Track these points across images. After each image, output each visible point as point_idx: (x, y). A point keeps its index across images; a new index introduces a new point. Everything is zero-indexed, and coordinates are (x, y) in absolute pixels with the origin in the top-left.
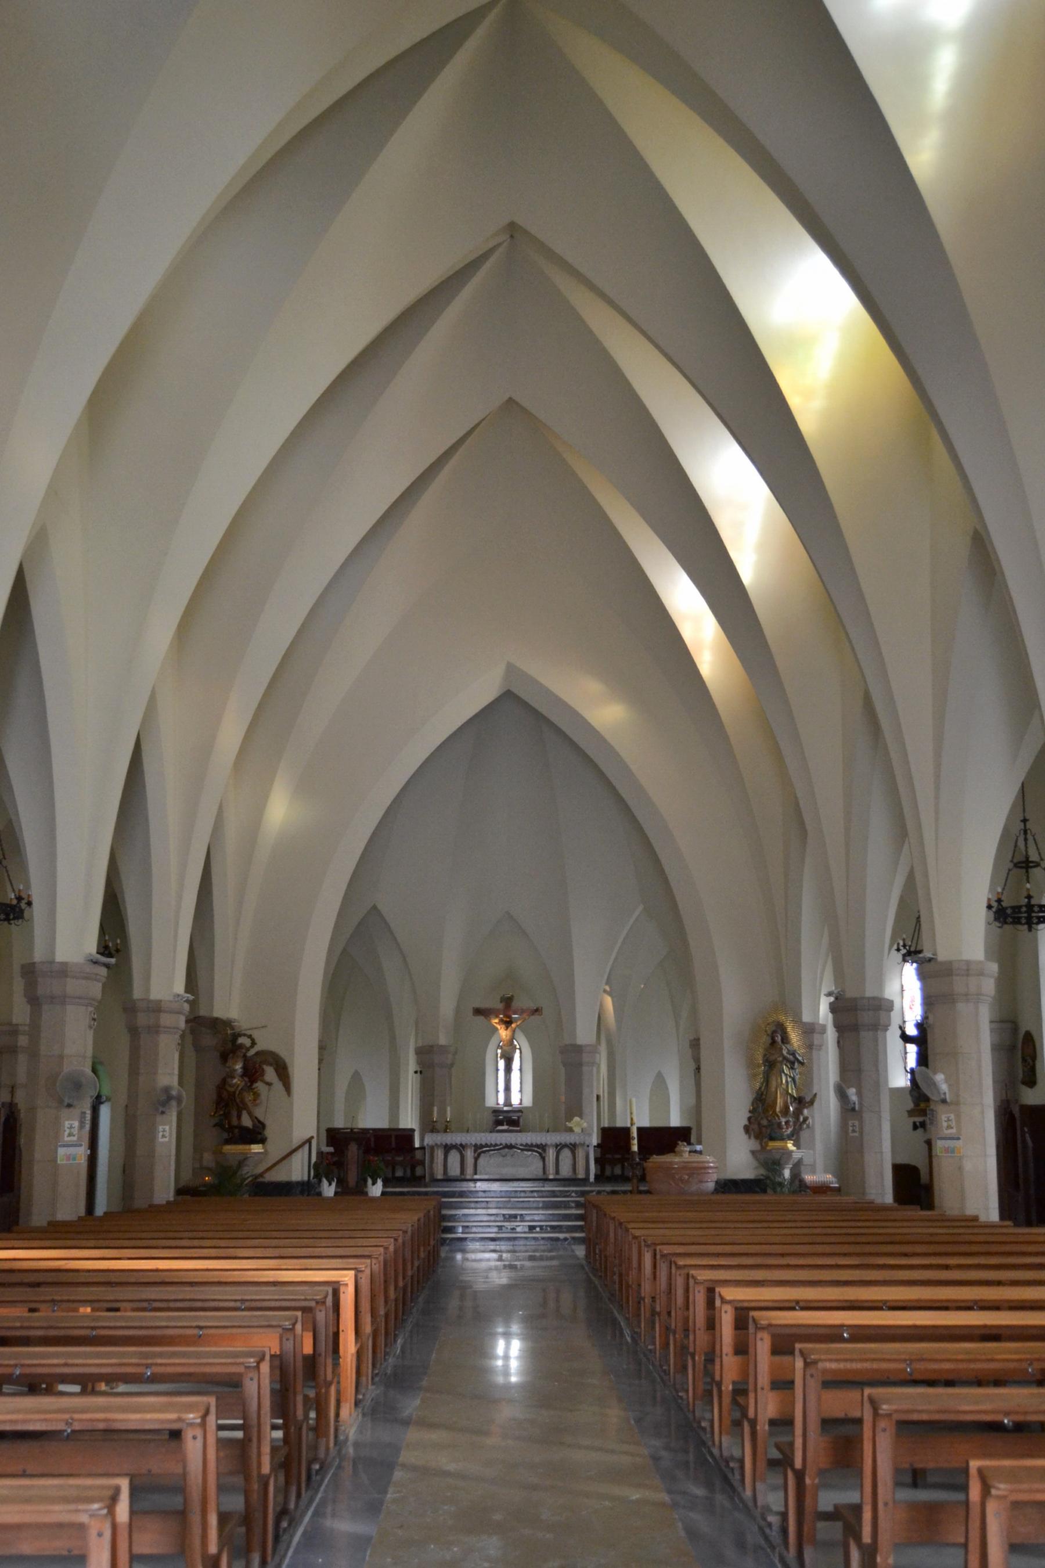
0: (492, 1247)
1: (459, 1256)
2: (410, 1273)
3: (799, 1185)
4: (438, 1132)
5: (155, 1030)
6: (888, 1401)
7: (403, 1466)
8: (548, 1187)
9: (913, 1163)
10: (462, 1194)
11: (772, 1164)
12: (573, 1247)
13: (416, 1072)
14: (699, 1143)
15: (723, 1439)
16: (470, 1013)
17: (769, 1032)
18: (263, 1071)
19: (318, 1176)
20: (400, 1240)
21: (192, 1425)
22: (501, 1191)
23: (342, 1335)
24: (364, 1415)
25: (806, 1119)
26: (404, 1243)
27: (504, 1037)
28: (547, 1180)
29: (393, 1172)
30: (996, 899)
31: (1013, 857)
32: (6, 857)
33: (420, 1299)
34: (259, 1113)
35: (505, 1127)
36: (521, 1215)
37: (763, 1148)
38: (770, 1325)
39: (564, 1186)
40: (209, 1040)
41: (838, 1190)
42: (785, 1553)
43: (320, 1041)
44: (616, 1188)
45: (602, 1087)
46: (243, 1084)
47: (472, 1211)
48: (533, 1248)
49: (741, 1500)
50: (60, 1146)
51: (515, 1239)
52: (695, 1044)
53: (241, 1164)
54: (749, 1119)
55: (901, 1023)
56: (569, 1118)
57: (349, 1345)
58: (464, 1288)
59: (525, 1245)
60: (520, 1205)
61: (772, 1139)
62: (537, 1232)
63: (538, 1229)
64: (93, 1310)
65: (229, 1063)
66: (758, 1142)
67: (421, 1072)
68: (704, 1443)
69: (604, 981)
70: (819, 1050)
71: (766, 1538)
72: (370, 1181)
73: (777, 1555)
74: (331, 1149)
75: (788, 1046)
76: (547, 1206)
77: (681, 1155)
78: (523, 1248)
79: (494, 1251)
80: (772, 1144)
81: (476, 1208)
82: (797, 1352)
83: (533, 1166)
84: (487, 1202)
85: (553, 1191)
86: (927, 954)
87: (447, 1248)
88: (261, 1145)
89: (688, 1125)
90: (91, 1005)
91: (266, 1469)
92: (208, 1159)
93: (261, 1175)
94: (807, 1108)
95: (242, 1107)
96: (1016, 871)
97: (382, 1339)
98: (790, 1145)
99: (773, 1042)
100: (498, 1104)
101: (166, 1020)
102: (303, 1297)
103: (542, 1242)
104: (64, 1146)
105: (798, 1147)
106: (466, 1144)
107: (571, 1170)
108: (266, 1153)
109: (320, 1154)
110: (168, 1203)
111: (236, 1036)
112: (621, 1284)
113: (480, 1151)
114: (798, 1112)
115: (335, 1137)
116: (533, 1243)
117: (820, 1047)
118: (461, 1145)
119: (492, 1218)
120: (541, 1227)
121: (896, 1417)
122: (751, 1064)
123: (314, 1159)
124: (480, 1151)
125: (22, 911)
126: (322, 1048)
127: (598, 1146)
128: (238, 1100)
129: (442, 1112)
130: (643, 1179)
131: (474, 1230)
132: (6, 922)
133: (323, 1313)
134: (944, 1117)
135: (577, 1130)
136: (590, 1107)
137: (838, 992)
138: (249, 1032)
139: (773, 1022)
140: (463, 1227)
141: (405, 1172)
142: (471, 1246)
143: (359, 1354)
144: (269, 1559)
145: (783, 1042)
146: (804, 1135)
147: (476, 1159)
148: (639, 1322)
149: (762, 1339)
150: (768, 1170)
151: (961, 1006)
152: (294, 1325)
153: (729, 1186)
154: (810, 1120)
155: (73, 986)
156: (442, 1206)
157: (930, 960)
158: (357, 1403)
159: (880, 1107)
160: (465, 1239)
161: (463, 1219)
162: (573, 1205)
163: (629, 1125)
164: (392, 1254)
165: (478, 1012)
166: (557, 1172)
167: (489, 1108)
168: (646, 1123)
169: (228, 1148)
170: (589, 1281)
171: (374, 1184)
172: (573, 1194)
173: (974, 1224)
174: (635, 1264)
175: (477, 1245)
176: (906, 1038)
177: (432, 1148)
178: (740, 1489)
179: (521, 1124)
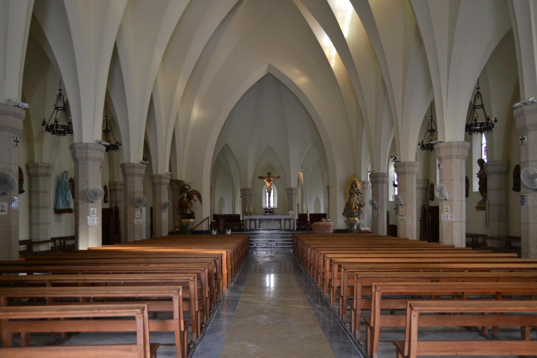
0: (265, 250)
1: (255, 253)
2: (240, 255)
3: (360, 231)
4: (248, 215)
5: (160, 184)
6: (360, 275)
7: (241, 301)
8: (282, 232)
9: (395, 224)
10: (255, 234)
11: (351, 225)
12: (290, 250)
13: (240, 197)
14: (329, 218)
15: (327, 294)
16: (257, 178)
17: (351, 184)
18: (193, 197)
19: (211, 229)
20: (238, 245)
21: (191, 280)
22: (267, 233)
23: (223, 268)
24: (229, 291)
25: (362, 211)
26: (239, 246)
27: (268, 185)
28: (281, 230)
29: (234, 228)
30: (421, 142)
31: (427, 128)
33: (244, 263)
34: (192, 209)
35: (269, 214)
36: (274, 240)
37: (348, 220)
38: (338, 262)
39: (287, 232)
40: (176, 187)
41: (371, 232)
42: (351, 333)
43: (210, 187)
44: (303, 232)
45: (299, 201)
46: (187, 200)
47: (258, 239)
48: (277, 250)
49: (330, 308)
50: (135, 219)
51: (272, 247)
52: (328, 188)
53: (187, 225)
54: (344, 211)
55: (393, 181)
56: (289, 211)
57: (225, 271)
58: (256, 262)
59: (275, 249)
60: (272, 237)
61: (351, 217)
62: (279, 245)
63: (279, 244)
65: (183, 194)
66: (347, 218)
67: (242, 197)
68: (322, 296)
69: (300, 168)
70: (366, 189)
71: (335, 315)
72: (227, 230)
73: (337, 318)
74: (215, 221)
75: (357, 188)
76: (281, 238)
77: (322, 222)
78: (274, 250)
80: (351, 218)
81: (260, 238)
82: (342, 267)
83: (277, 225)
84: (263, 236)
85: (283, 233)
86: (398, 160)
87: (251, 250)
88: (193, 219)
89: (325, 213)
90: (142, 176)
91: (207, 296)
92: (177, 224)
93: (194, 228)
94: (362, 207)
95: (187, 208)
96: (428, 133)
97: (233, 272)
98: (357, 219)
99: (352, 187)
100: (266, 207)
101: (163, 180)
102: (213, 257)
103: (280, 248)
104: (136, 219)
105: (359, 219)
107: (289, 227)
108: (195, 221)
109: (211, 222)
110: (167, 236)
111: (185, 185)
112: (302, 258)
113: (261, 221)
114: (359, 209)
115: (216, 217)
116: (277, 248)
117: (367, 188)
118: (255, 219)
119: (265, 241)
122: (345, 194)
123: (210, 223)
124: (261, 221)
126: (211, 189)
127: (298, 219)
128: (186, 205)
129: (249, 209)
130: (311, 230)
131: (259, 245)
132: (113, 151)
133: (218, 261)
134: (401, 210)
135: (291, 214)
136: (295, 207)
137: (372, 171)
138: (188, 184)
139: (352, 181)
140: (256, 244)
141: (238, 228)
142: (258, 249)
143: (228, 274)
144: (208, 318)
145: (355, 186)
146: (361, 216)
147: (260, 223)
148: (307, 268)
149: (335, 266)
150: (350, 226)
151: (407, 176)
152: (212, 262)
153: (338, 231)
154: (363, 211)
155: (136, 171)
156: (249, 238)
157: (399, 161)
158: (227, 287)
159: (383, 207)
160: (257, 247)
161: (256, 241)
162: (289, 237)
163: (307, 213)
164: (236, 249)
165: (260, 177)
166: (285, 227)
167: (264, 208)
168: (313, 212)
169: (183, 220)
170: (294, 259)
171: (228, 231)
172: (290, 234)
174: (306, 251)
175: (260, 249)
176: (395, 186)
177: (246, 220)
178: (330, 305)
179: (274, 213)
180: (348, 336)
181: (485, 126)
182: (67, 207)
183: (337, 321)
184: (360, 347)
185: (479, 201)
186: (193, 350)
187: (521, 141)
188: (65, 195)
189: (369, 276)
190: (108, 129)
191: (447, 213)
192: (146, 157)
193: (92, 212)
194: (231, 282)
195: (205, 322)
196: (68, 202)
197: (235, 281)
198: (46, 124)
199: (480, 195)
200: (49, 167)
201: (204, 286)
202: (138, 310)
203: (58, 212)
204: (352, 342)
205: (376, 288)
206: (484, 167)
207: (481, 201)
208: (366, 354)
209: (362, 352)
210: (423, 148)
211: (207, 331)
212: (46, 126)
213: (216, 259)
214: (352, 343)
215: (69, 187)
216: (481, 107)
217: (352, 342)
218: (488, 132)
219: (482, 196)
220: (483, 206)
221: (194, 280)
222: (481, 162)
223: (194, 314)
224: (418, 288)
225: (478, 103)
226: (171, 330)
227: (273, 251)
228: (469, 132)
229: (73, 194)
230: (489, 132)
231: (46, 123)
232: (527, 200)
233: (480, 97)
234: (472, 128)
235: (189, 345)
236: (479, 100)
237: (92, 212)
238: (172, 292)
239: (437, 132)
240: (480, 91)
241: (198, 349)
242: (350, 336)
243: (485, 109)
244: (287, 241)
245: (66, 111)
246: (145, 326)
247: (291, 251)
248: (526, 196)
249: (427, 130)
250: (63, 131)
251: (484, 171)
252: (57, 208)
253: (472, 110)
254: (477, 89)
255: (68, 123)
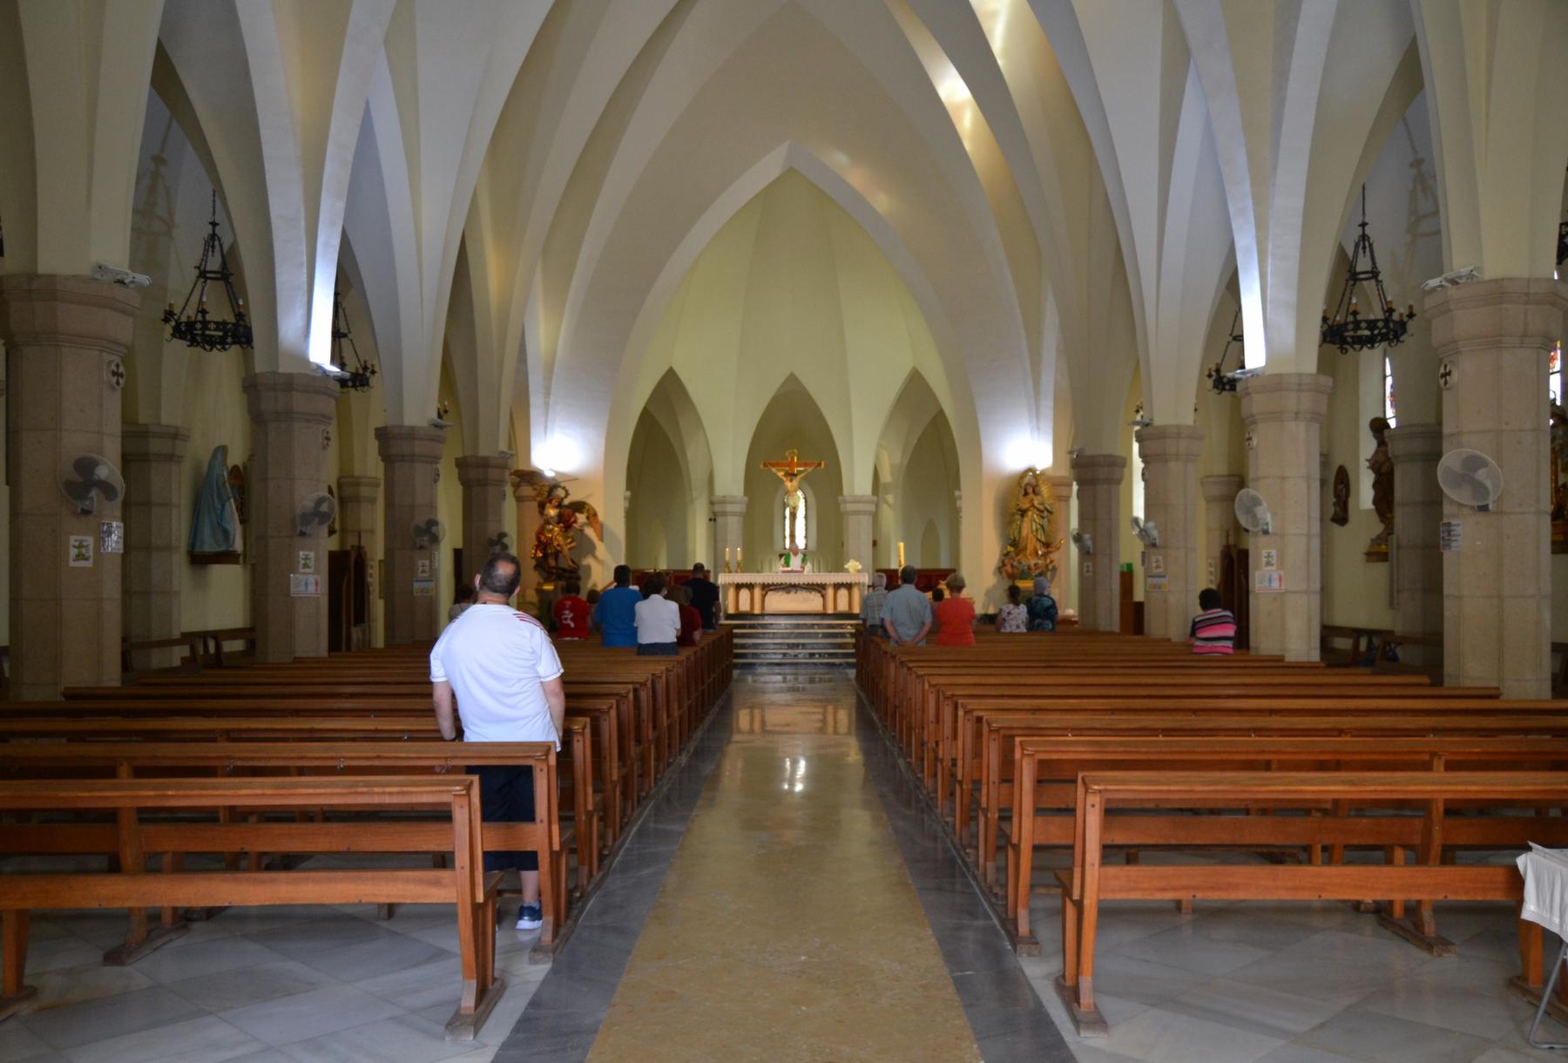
0: (777, 671)
1: (750, 678)
31: (1232, 331)
32: (351, 330)
41: (1076, 622)
42: (976, 872)
50: (417, 581)
51: (797, 664)
63: (817, 656)
64: (1027, 485)
79: (778, 674)
91: (615, 777)
100: (785, 549)
106: (756, 584)
118: (751, 584)
119: (778, 646)
120: (820, 654)
121: (1002, 732)
125: (368, 379)
133: (645, 692)
147: (764, 597)
160: (754, 664)
172: (849, 627)
173: (1280, 664)
175: (764, 670)
180: (970, 879)
181: (1381, 329)
182: (223, 548)
183: (950, 845)
184: (993, 900)
185: (1374, 536)
186: (580, 904)
187: (1444, 379)
188: (219, 512)
189: (1018, 726)
190: (339, 330)
191: (1269, 568)
192: (445, 406)
193: (302, 562)
194: (680, 752)
195: (610, 843)
196: (226, 533)
197: (692, 751)
198: (176, 317)
199: (1375, 518)
200: (176, 435)
201: (608, 751)
202: (458, 788)
203: (200, 560)
204: (978, 892)
205: (1023, 749)
206: (1386, 440)
207: (1379, 537)
208: (1004, 916)
209: (995, 911)
210: (1220, 387)
211: (614, 865)
212: (173, 323)
213: (638, 686)
214: (976, 894)
215: (229, 490)
216: (1371, 275)
217: (978, 892)
218: (1389, 345)
219: (1382, 521)
220: (1385, 551)
221: (583, 734)
222: (1379, 426)
223: (584, 818)
224: (1122, 749)
225: (1363, 265)
226: (529, 849)
227: (802, 674)
228: (1338, 346)
229: (243, 510)
230: (1393, 344)
231: (175, 315)
232: (1457, 535)
233: (1367, 250)
234: (1346, 334)
235: (570, 892)
236: (1365, 256)
237: (302, 562)
238: (532, 754)
239: (1325, 319)
240: (1368, 230)
241: (592, 905)
242: (975, 878)
243: (1381, 281)
244: (840, 646)
245: (230, 283)
246: (473, 825)
247: (852, 673)
248: (1454, 525)
249: (1231, 335)
250: (220, 337)
251: (1386, 453)
252: (197, 549)
253: (1346, 284)
254: (1360, 225)
255: (236, 315)
